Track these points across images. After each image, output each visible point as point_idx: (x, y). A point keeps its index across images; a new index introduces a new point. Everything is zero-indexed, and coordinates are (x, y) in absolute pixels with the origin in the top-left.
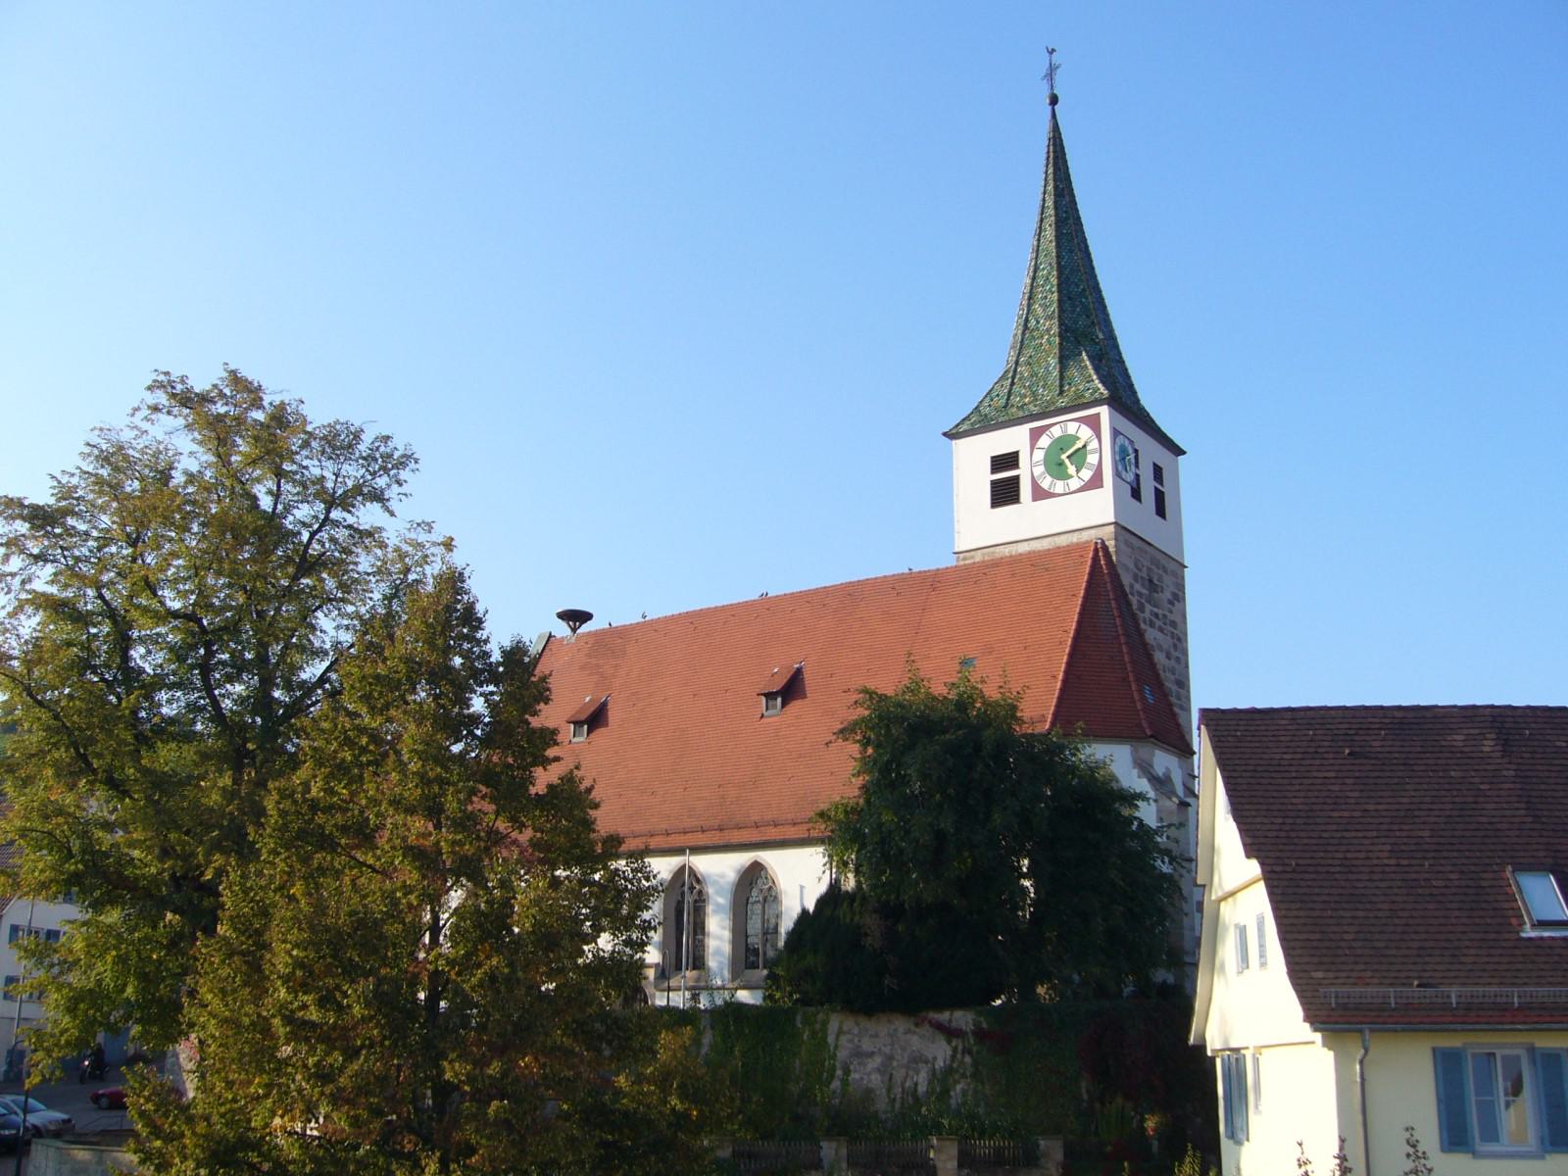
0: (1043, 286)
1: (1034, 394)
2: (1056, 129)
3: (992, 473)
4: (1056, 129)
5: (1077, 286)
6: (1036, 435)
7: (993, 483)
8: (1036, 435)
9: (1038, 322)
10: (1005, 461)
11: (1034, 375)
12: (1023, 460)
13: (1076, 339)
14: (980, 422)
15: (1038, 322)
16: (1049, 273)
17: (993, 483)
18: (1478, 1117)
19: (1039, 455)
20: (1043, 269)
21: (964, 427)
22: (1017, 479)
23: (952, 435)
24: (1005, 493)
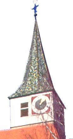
0: (34, 61)
1: (32, 89)
2: (36, 30)
3: (21, 107)
4: (36, 30)
5: (42, 62)
6: (33, 99)
7: (28, 106)
8: (33, 99)
9: (32, 71)
10: (25, 105)
11: (32, 83)
12: (29, 104)
13: (42, 75)
14: (18, 95)
15: (32, 71)
16: (35, 59)
17: (28, 106)
18: (25, 107)
19: (34, 103)
20: (34, 57)
21: (13, 96)
22: (28, 109)
23: (10, 98)
24: (24, 113)
